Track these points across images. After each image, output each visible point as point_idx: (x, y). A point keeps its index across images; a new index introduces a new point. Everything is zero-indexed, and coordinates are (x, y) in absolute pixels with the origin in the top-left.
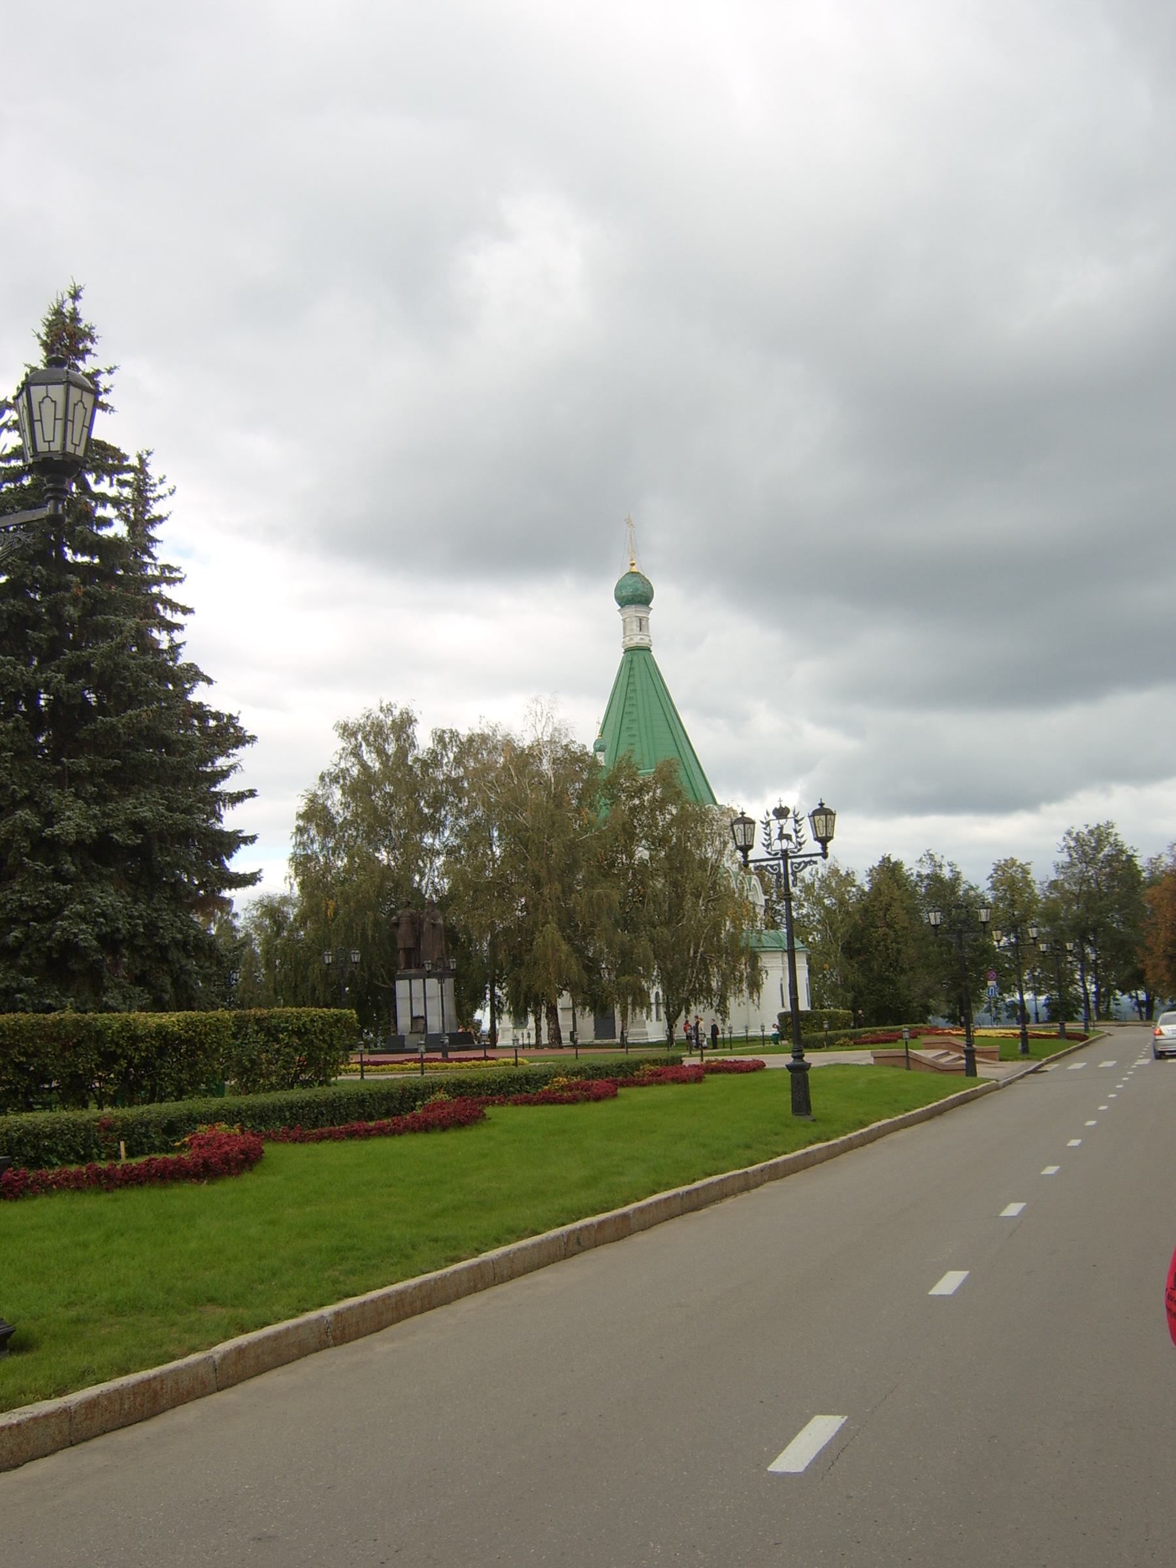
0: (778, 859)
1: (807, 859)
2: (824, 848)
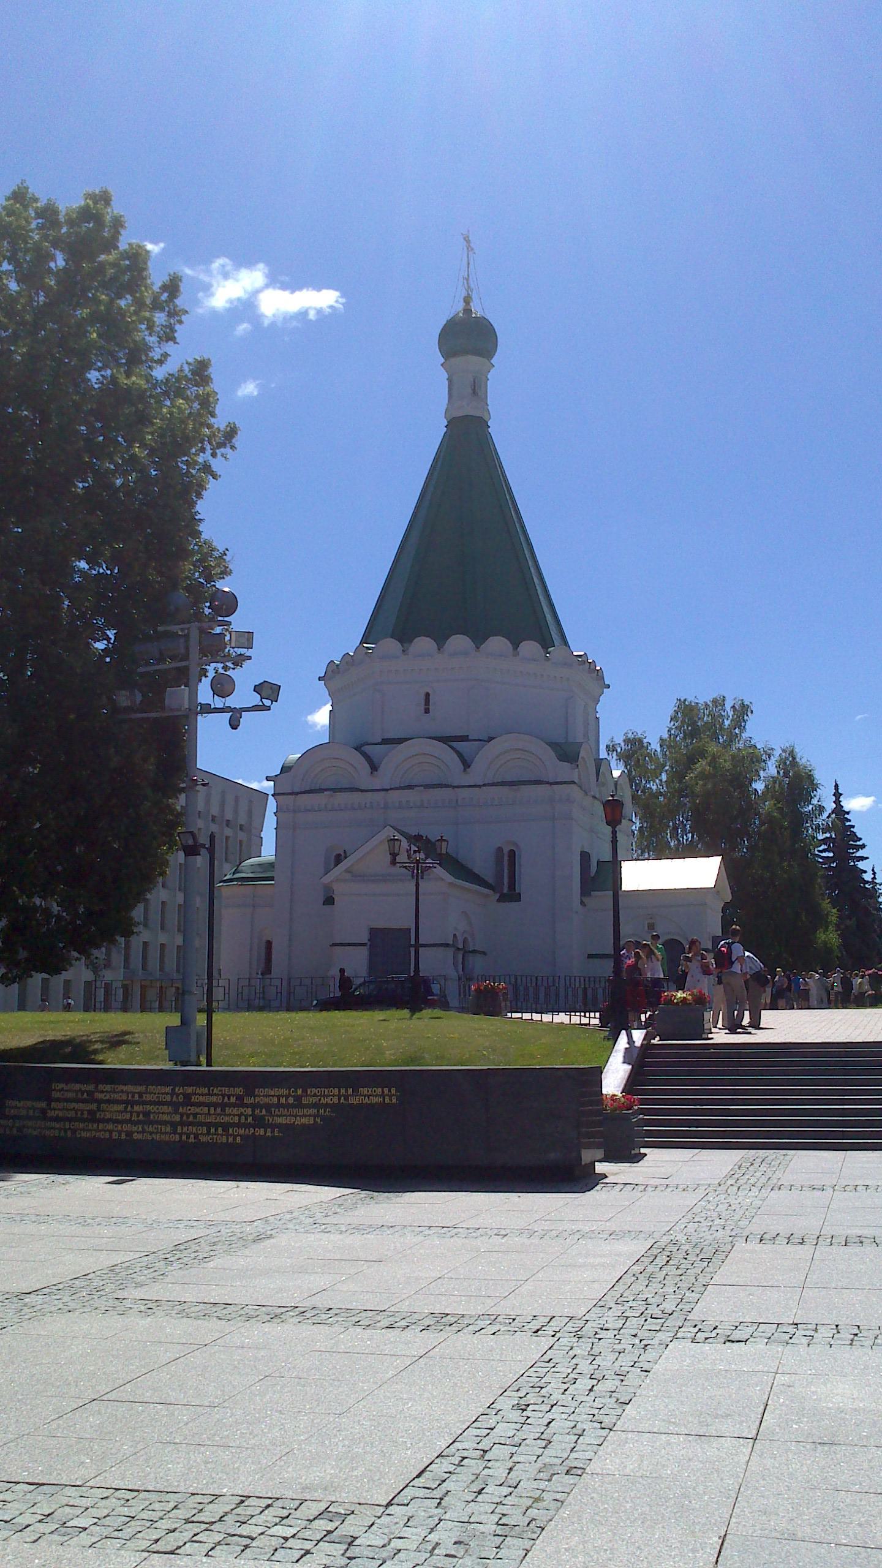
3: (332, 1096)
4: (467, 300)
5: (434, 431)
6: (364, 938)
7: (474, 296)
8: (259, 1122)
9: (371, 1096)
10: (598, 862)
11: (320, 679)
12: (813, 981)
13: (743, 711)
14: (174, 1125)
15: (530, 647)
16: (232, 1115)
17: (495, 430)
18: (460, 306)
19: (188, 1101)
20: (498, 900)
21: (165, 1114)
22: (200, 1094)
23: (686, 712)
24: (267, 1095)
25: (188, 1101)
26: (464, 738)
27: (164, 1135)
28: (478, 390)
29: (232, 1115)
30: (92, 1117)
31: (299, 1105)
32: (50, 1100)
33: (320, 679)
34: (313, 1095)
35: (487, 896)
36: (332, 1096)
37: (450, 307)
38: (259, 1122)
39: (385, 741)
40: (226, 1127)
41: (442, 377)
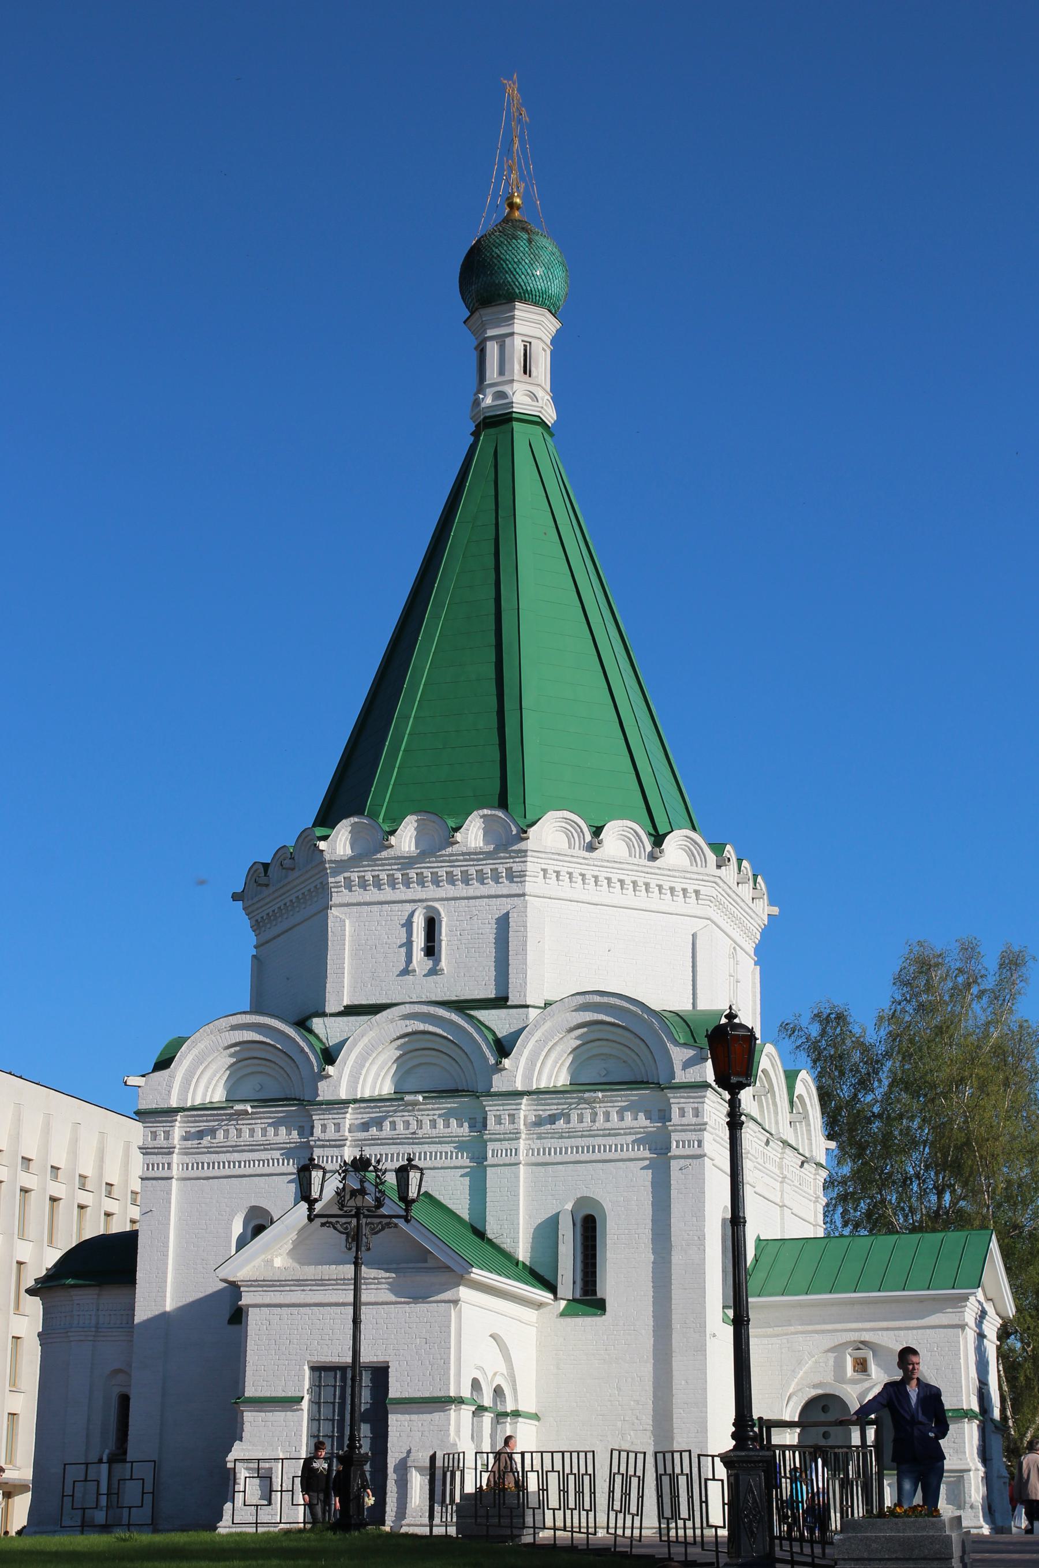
0: (352, 1216)
1: (385, 1221)
2: (407, 1210)
10: (759, 1240)
11: (236, 897)
20: (563, 1314)
23: (920, 972)
26: (501, 1002)
33: (236, 897)
35: (540, 1305)
39: (351, 1011)
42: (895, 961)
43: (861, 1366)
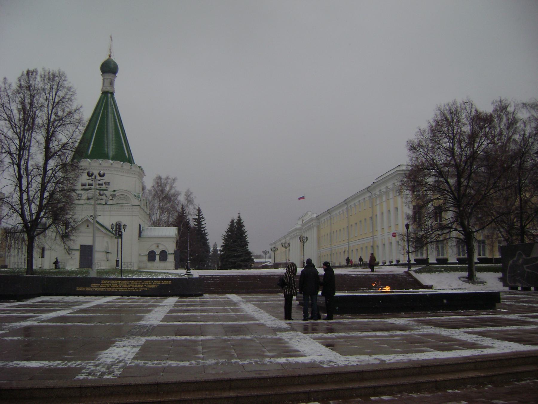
3: (159, 282)
4: (110, 56)
5: (98, 95)
6: (79, 248)
7: (112, 55)
8: (145, 287)
9: (167, 282)
12: (90, 258)
13: (174, 180)
14: (127, 288)
15: (127, 165)
16: (139, 286)
17: (116, 96)
18: (108, 57)
19: (130, 283)
21: (126, 286)
22: (132, 282)
24: (145, 282)
25: (130, 283)
27: (126, 290)
28: (112, 84)
29: (139, 286)
30: (110, 287)
31: (152, 284)
32: (101, 284)
34: (155, 282)
35: (112, 237)
36: (159, 282)
37: (104, 58)
38: (145, 287)
40: (138, 288)
41: (101, 78)
42: (155, 176)
43: (158, 247)
